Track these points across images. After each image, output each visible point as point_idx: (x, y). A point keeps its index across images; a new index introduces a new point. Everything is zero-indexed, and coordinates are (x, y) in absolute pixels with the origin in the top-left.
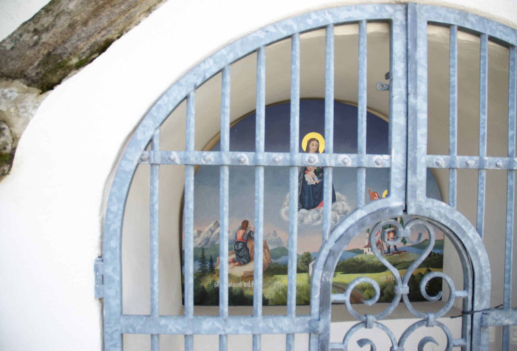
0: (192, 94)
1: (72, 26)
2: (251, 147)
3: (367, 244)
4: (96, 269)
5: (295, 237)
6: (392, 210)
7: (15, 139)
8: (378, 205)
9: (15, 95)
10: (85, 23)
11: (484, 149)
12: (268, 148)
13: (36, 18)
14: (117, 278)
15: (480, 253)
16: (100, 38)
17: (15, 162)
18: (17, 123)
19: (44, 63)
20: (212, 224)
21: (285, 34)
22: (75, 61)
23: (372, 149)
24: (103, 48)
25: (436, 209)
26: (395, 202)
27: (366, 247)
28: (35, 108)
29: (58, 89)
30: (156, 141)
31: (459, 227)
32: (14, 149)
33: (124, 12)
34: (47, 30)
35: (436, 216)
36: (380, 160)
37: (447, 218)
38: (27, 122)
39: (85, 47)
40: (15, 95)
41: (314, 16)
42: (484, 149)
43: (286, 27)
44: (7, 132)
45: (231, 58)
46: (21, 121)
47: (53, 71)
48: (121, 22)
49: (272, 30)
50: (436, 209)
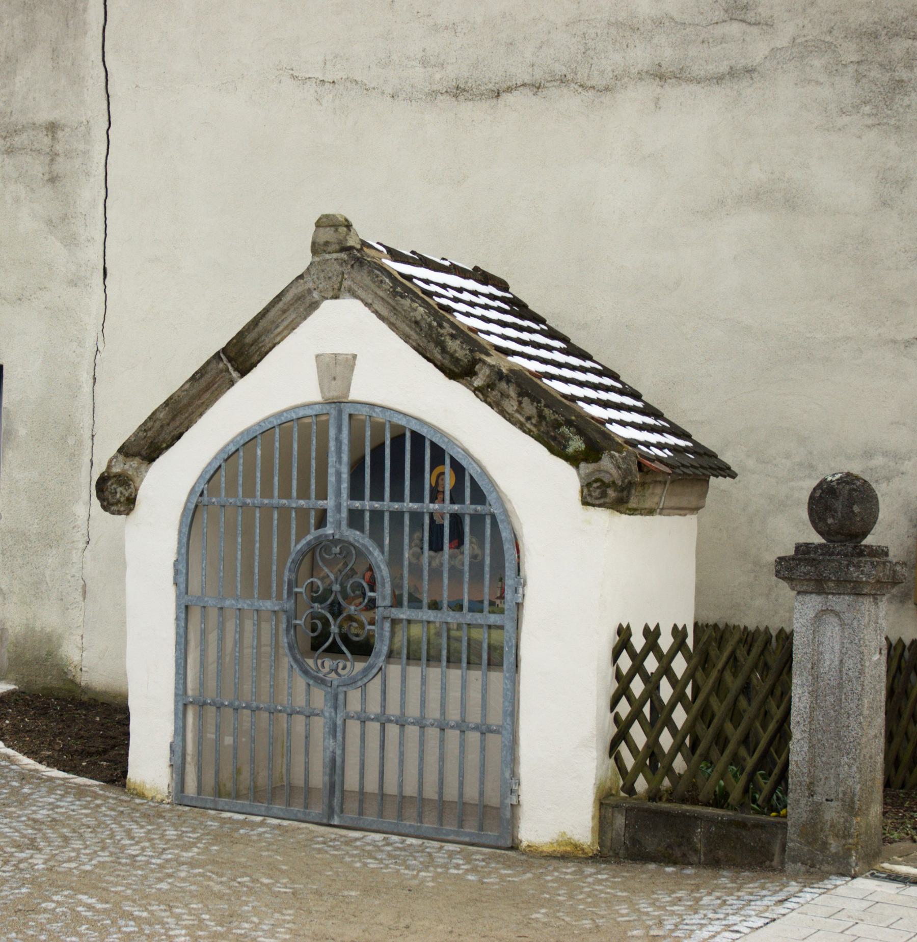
0: (223, 465)
1: (162, 427)
2: (362, 498)
3: (499, 595)
4: (175, 566)
5: (426, 583)
6: (326, 536)
7: (137, 490)
8: (321, 531)
9: (136, 465)
10: (168, 425)
11: (468, 501)
12: (372, 499)
13: (145, 423)
14: (184, 571)
15: (382, 567)
16: (176, 433)
17: (137, 503)
18: (137, 480)
19: (149, 447)
20: (341, 565)
21: (270, 426)
22: (164, 445)
23: (393, 499)
24: (179, 437)
25: (353, 535)
26: (329, 530)
27: (498, 598)
28: (146, 472)
29: (157, 460)
30: (205, 492)
31: (367, 549)
32: (136, 496)
33: (187, 418)
34: (150, 429)
35: (351, 539)
36: (321, 503)
37: (358, 542)
38: (142, 480)
39: (169, 438)
40: (136, 465)
41: (285, 414)
42: (468, 501)
43: (270, 422)
44: (132, 486)
45: (242, 442)
46: (139, 480)
47: (154, 451)
48: (186, 423)
49: (263, 424)
50: (353, 535)
